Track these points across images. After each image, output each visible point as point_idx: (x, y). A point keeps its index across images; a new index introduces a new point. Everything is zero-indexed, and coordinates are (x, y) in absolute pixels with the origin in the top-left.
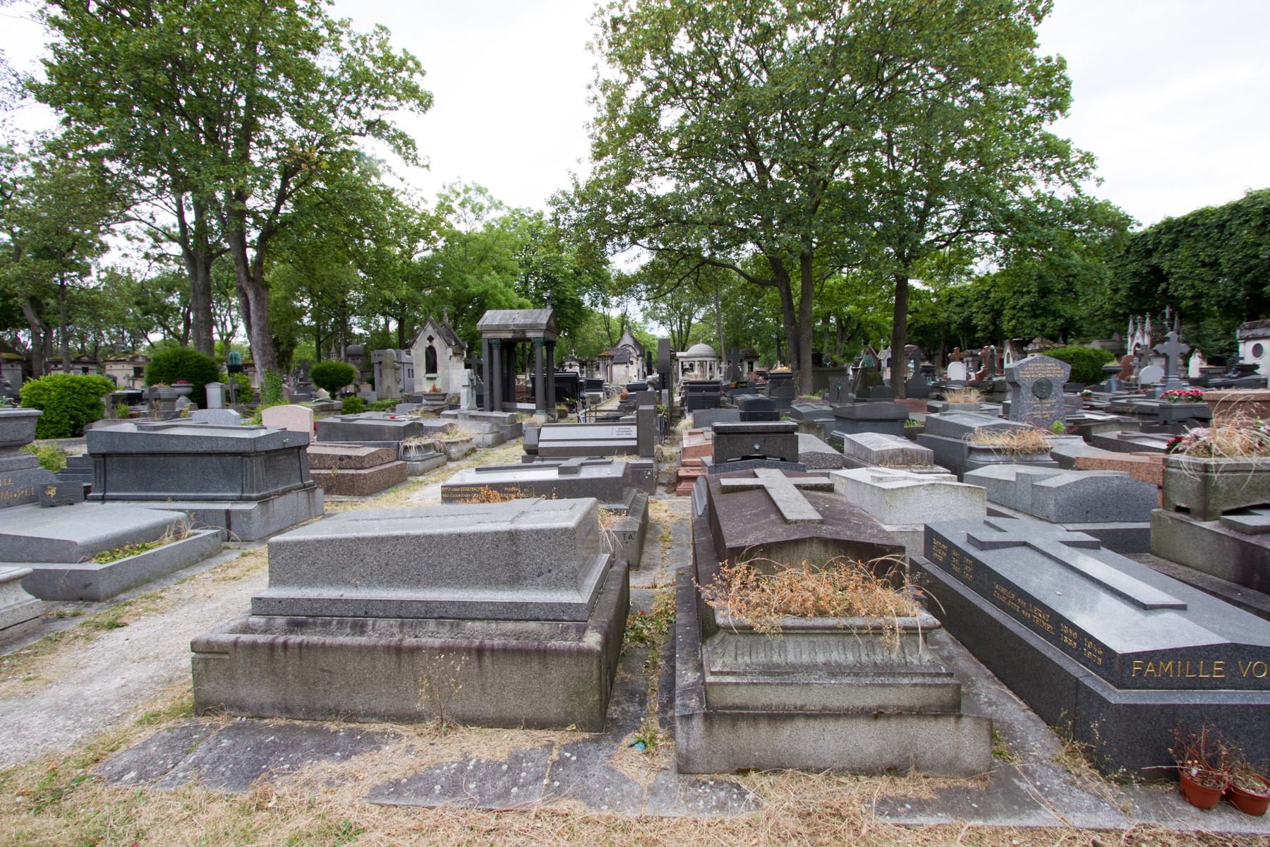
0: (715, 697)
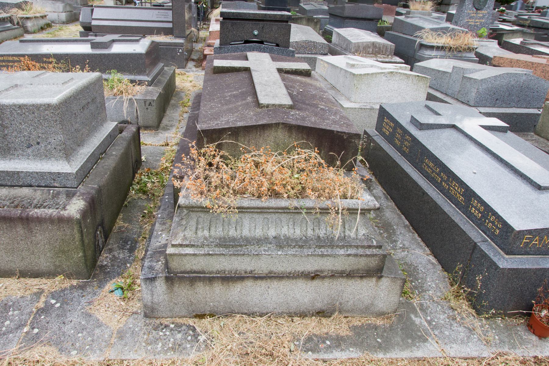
0: (174, 264)
